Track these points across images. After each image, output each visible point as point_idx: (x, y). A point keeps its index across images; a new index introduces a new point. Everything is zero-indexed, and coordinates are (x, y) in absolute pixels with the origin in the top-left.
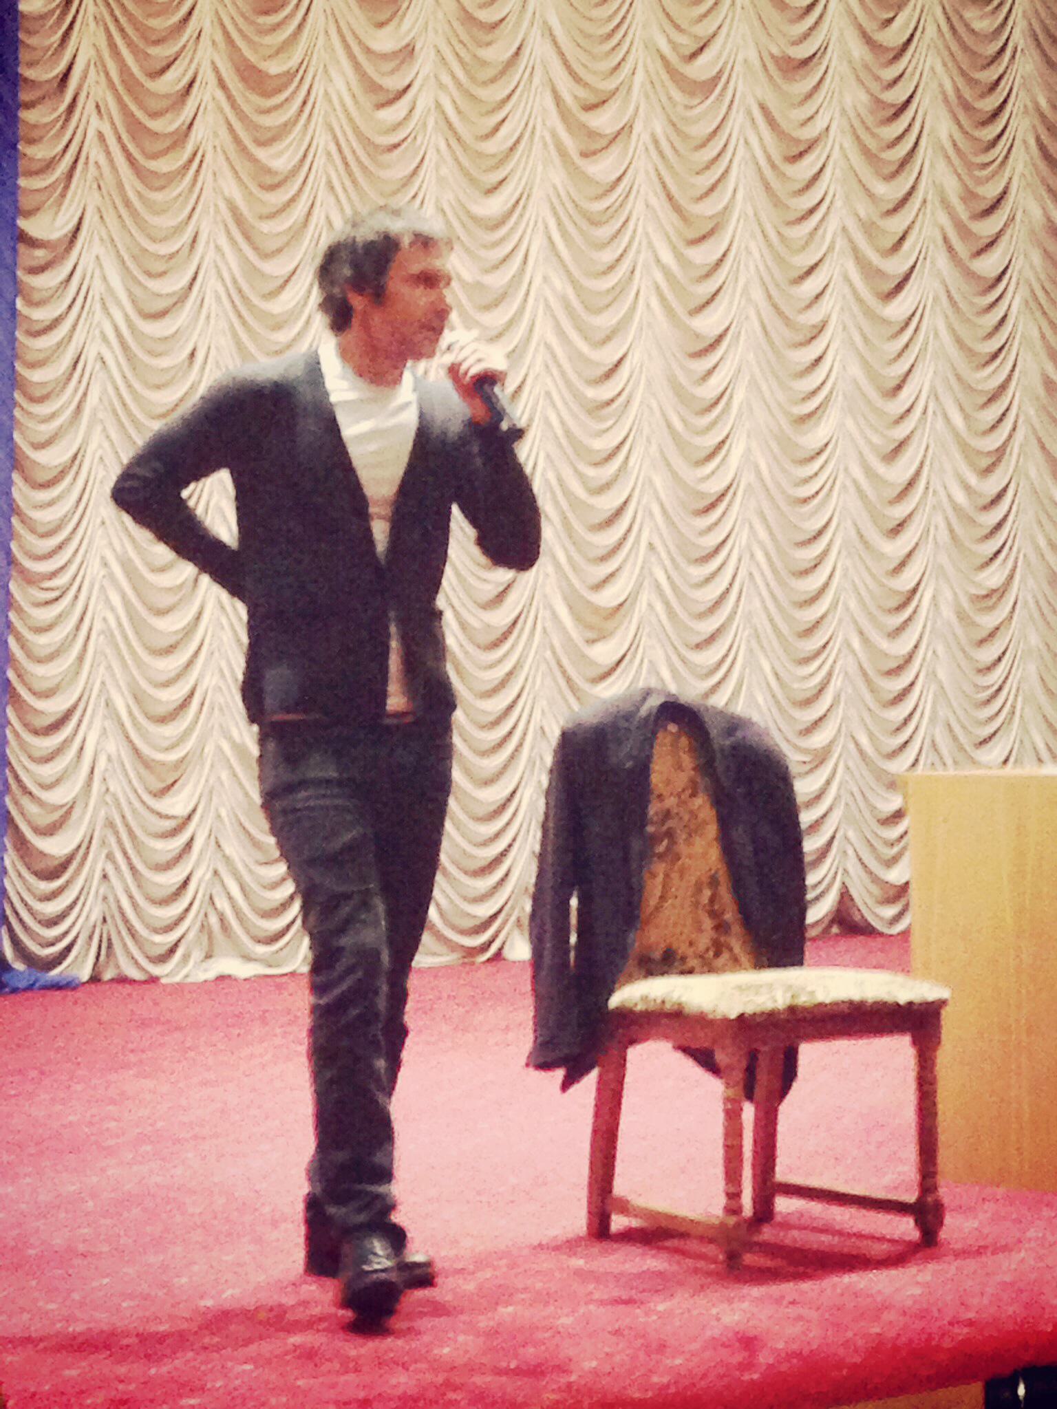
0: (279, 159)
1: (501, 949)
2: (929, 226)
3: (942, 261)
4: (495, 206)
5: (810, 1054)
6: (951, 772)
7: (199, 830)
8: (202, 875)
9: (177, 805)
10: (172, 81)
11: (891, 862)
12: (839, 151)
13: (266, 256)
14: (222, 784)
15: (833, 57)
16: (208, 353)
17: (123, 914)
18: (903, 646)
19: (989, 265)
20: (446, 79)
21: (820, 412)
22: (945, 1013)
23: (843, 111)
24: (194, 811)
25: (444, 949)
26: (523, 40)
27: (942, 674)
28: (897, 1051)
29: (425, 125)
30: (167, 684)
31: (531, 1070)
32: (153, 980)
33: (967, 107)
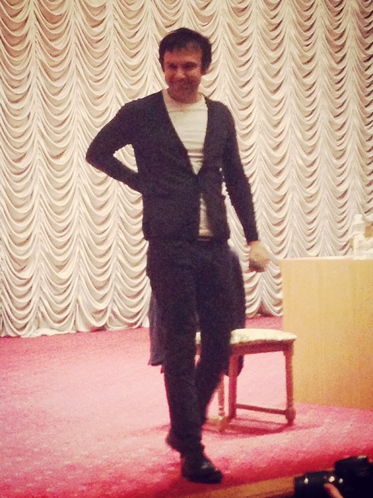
0: (59, 45)
1: (142, 324)
2: (288, 67)
3: (293, 79)
4: (135, 61)
5: (249, 359)
6: (299, 259)
7: (34, 283)
8: (35, 299)
9: (26, 274)
10: (19, 19)
11: (278, 291)
12: (256, 41)
13: (55, 80)
14: (42, 267)
15: (253, 9)
16: (34, 115)
17: (7, 314)
18: (281, 215)
19: (309, 81)
20: (117, 17)
21: (251, 132)
22: (295, 344)
23: (258, 28)
24: (32, 276)
25: (121, 324)
26: (144, 3)
27: (295, 225)
28: (279, 356)
29: (110, 33)
30: (22, 232)
31: (150, 366)
32: (19, 337)
33: (300, 24)
